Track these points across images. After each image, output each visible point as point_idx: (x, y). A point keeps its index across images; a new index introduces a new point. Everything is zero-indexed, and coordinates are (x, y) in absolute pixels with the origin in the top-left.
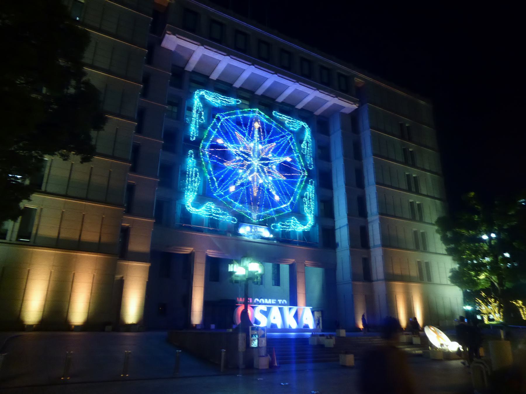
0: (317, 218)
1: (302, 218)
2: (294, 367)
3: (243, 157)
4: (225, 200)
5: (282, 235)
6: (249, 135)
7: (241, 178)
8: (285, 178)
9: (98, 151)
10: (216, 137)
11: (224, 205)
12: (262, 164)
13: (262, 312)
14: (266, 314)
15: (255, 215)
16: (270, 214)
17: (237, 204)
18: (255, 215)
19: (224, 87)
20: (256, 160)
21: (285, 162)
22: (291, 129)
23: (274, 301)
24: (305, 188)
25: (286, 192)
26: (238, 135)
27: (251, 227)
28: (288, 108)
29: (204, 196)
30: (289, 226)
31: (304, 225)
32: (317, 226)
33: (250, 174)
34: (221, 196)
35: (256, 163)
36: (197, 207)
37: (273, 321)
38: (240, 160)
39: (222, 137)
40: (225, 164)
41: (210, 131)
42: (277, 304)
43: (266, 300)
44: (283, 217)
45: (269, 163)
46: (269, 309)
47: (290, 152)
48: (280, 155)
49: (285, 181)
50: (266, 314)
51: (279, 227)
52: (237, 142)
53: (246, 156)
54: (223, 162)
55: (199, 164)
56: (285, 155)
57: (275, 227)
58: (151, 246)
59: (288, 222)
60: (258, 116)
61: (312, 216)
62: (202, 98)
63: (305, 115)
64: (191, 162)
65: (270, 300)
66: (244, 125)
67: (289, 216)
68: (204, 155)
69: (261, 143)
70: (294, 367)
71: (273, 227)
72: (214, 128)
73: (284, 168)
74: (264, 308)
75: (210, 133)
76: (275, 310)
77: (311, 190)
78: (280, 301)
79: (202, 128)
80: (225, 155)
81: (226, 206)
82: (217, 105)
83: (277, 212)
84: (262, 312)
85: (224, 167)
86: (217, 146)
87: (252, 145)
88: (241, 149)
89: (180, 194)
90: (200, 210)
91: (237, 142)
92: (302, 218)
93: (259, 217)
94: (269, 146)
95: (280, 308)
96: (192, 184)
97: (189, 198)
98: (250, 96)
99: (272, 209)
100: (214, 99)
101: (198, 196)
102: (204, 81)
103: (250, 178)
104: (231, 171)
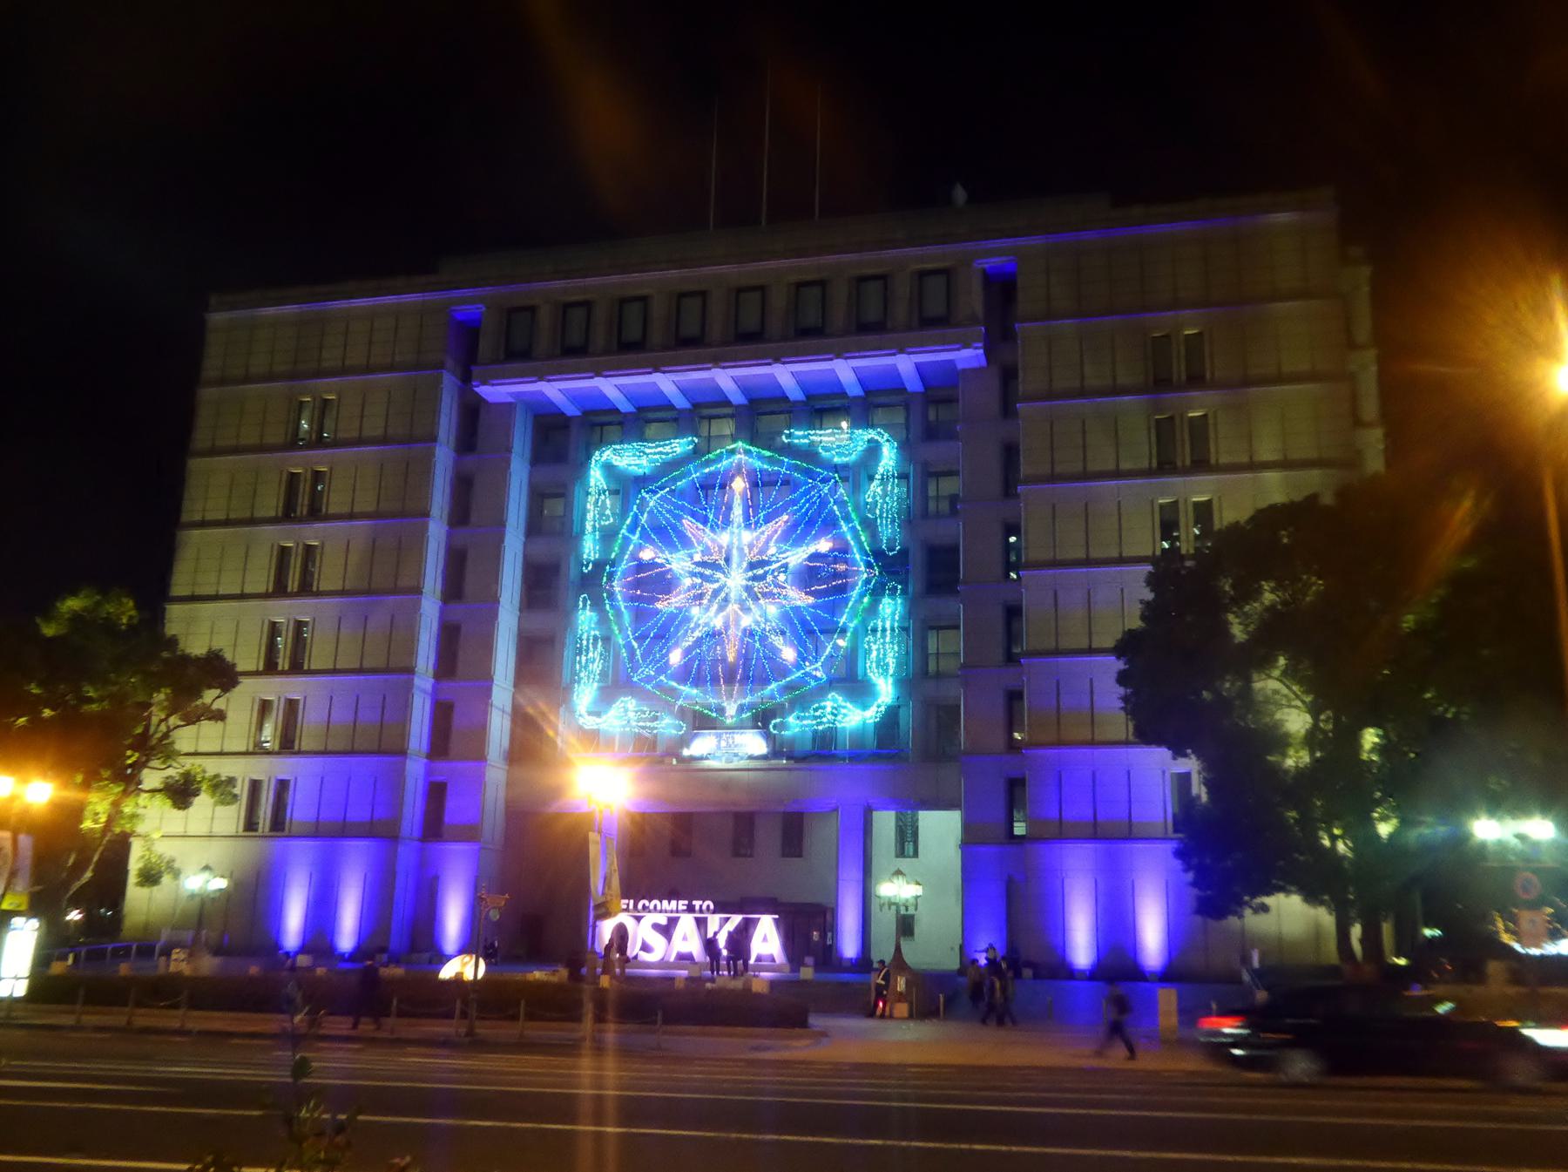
3: (702, 575)
4: (659, 686)
5: (814, 740)
6: (716, 516)
7: (697, 625)
8: (811, 600)
9: (239, 668)
10: (640, 548)
11: (658, 699)
13: (656, 927)
14: (666, 930)
15: (731, 709)
16: (772, 697)
17: (686, 689)
18: (731, 709)
19: (640, 420)
21: (815, 556)
22: (837, 460)
23: (682, 904)
24: (872, 610)
25: (808, 631)
26: (688, 523)
27: (719, 736)
28: (822, 406)
34: (649, 679)
35: (735, 580)
36: (598, 714)
37: (685, 948)
38: (694, 586)
39: (652, 542)
40: (659, 605)
41: (625, 538)
42: (691, 909)
43: (665, 902)
44: (802, 697)
45: (766, 573)
46: (673, 922)
47: (830, 525)
48: (799, 542)
49: (814, 606)
50: (666, 930)
51: (795, 726)
52: (686, 542)
53: (708, 572)
54: (654, 600)
55: (603, 620)
56: (816, 538)
57: (782, 726)
58: (699, 814)
59: (816, 710)
60: (740, 457)
61: (891, 680)
62: (609, 468)
63: (864, 406)
64: (585, 620)
65: (674, 903)
67: (821, 691)
68: (611, 596)
69: (748, 526)
71: (775, 727)
72: (632, 530)
73: (808, 576)
74: (662, 919)
75: (626, 540)
76: (687, 923)
78: (697, 903)
79: (608, 536)
80: (662, 582)
81: (659, 699)
82: (640, 472)
83: (790, 688)
84: (656, 927)
85: (657, 612)
86: (641, 566)
87: (724, 538)
88: (697, 558)
91: (686, 542)
93: (741, 709)
94: (768, 529)
95: (698, 920)
96: (586, 667)
99: (774, 685)
100: (631, 458)
101: (601, 689)
102: (604, 423)
103: (718, 623)
104: (672, 617)
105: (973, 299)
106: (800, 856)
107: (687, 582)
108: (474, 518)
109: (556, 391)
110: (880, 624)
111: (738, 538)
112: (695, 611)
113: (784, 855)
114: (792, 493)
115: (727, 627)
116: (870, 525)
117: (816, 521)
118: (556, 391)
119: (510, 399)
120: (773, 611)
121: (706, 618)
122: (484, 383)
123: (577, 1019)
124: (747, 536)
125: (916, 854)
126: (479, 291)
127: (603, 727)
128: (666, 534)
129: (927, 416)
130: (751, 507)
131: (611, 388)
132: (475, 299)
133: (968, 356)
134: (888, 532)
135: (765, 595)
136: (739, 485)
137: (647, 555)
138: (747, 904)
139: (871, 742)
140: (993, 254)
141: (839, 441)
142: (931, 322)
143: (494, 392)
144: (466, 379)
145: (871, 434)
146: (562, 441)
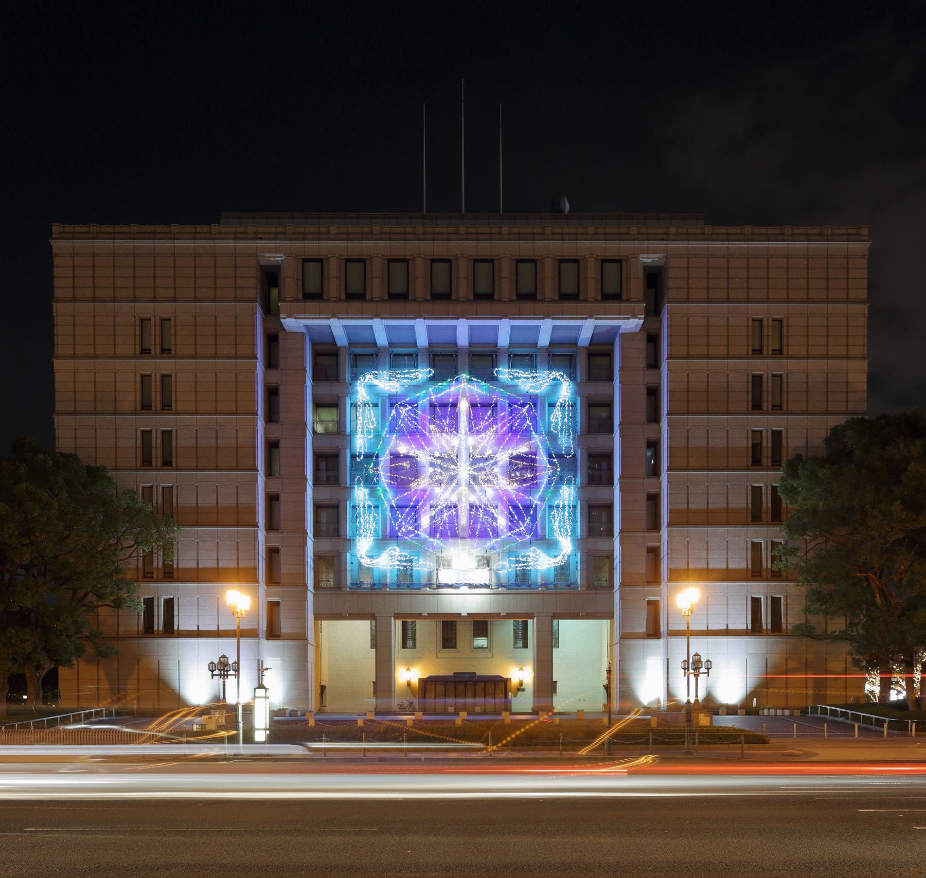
0: (579, 543)
1: (549, 545)
2: (811, 692)
5: (517, 575)
8: (516, 485)
12: (474, 470)
19: (400, 357)
20: (466, 466)
29: (388, 537)
30: (526, 562)
31: (556, 557)
32: (579, 554)
33: (453, 491)
35: (464, 471)
49: (518, 490)
55: (373, 494)
56: (518, 444)
59: (523, 557)
60: (465, 389)
61: (569, 539)
62: (371, 387)
63: (561, 355)
64: (360, 494)
66: (444, 410)
70: (811, 692)
77: (568, 494)
87: (455, 441)
88: (437, 454)
89: (348, 543)
90: (379, 560)
92: (549, 545)
97: (363, 547)
98: (444, 360)
100: (386, 382)
102: (367, 356)
103: (454, 499)
105: (636, 286)
106: (443, 647)
107: (496, 470)
108: (282, 416)
109: (339, 328)
110: (561, 503)
111: (462, 441)
112: (438, 490)
113: (443, 647)
114: (521, 414)
115: (459, 500)
116: (552, 437)
117: (517, 433)
118: (339, 328)
119: (304, 330)
120: (490, 493)
121: (443, 495)
122: (290, 316)
123: (238, 742)
124: (471, 440)
125: (414, 646)
126: (279, 243)
127: (375, 566)
128: (414, 434)
129: (591, 363)
130: (474, 419)
131: (380, 330)
132: (275, 252)
133: (632, 324)
134: (565, 442)
135: (485, 482)
136: (464, 406)
137: (403, 449)
138: (921, 691)
139: (552, 578)
140: (649, 255)
141: (532, 382)
142: (612, 297)
143: (291, 324)
144: (270, 311)
145: (556, 374)
146: (332, 366)
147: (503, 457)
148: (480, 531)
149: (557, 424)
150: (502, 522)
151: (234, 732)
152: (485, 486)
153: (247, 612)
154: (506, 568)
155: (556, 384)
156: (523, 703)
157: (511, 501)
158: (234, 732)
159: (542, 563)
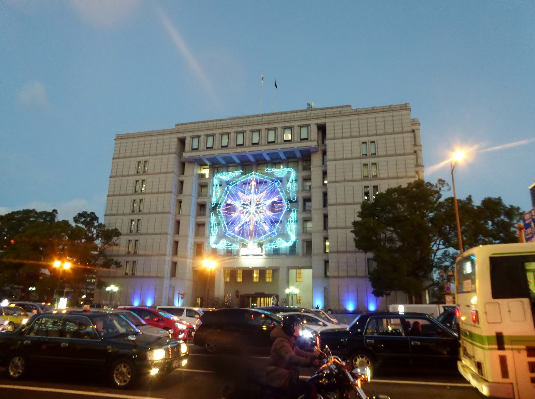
29: (222, 236)
33: (248, 216)
35: (252, 208)
60: (254, 176)
64: (213, 219)
103: (248, 220)
117: (274, 192)
120: (262, 217)
121: (244, 219)
124: (255, 197)
128: (233, 196)
135: (260, 212)
136: (253, 183)
137: (229, 202)
141: (280, 171)
145: (289, 169)
147: (269, 202)
148: (257, 232)
149: (289, 188)
150: (266, 228)
151: (428, 302)
152: (260, 214)
153: (156, 375)
154: (268, 247)
155: (289, 173)
156: (385, 292)
157: (270, 219)
158: (428, 302)
159: (284, 245)
